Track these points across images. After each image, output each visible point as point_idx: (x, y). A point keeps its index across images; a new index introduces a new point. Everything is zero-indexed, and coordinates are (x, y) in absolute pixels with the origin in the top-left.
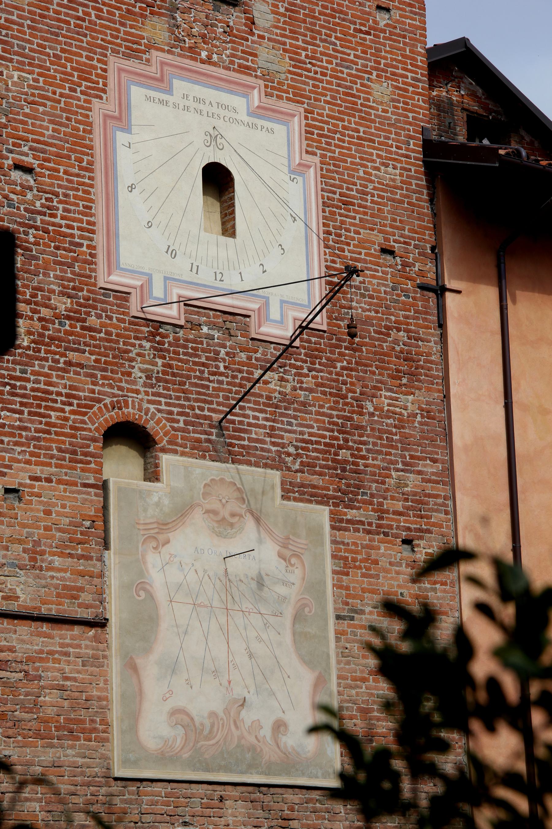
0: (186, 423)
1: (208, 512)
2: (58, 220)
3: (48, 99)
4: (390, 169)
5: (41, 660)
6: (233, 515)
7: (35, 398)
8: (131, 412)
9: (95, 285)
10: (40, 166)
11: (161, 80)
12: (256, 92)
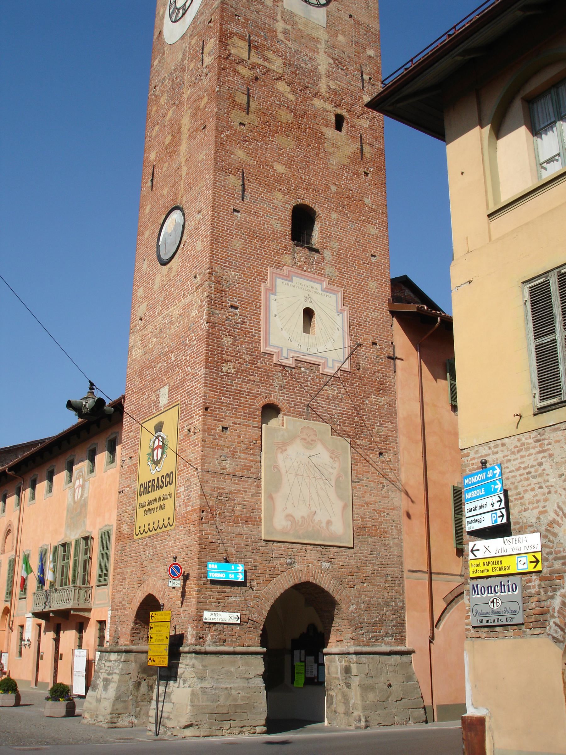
0: (295, 405)
1: (302, 439)
2: (247, 326)
3: (245, 282)
4: (376, 313)
5: (235, 493)
6: (312, 441)
7: (235, 393)
8: (272, 400)
9: (260, 351)
10: (241, 306)
11: (288, 277)
12: (325, 283)
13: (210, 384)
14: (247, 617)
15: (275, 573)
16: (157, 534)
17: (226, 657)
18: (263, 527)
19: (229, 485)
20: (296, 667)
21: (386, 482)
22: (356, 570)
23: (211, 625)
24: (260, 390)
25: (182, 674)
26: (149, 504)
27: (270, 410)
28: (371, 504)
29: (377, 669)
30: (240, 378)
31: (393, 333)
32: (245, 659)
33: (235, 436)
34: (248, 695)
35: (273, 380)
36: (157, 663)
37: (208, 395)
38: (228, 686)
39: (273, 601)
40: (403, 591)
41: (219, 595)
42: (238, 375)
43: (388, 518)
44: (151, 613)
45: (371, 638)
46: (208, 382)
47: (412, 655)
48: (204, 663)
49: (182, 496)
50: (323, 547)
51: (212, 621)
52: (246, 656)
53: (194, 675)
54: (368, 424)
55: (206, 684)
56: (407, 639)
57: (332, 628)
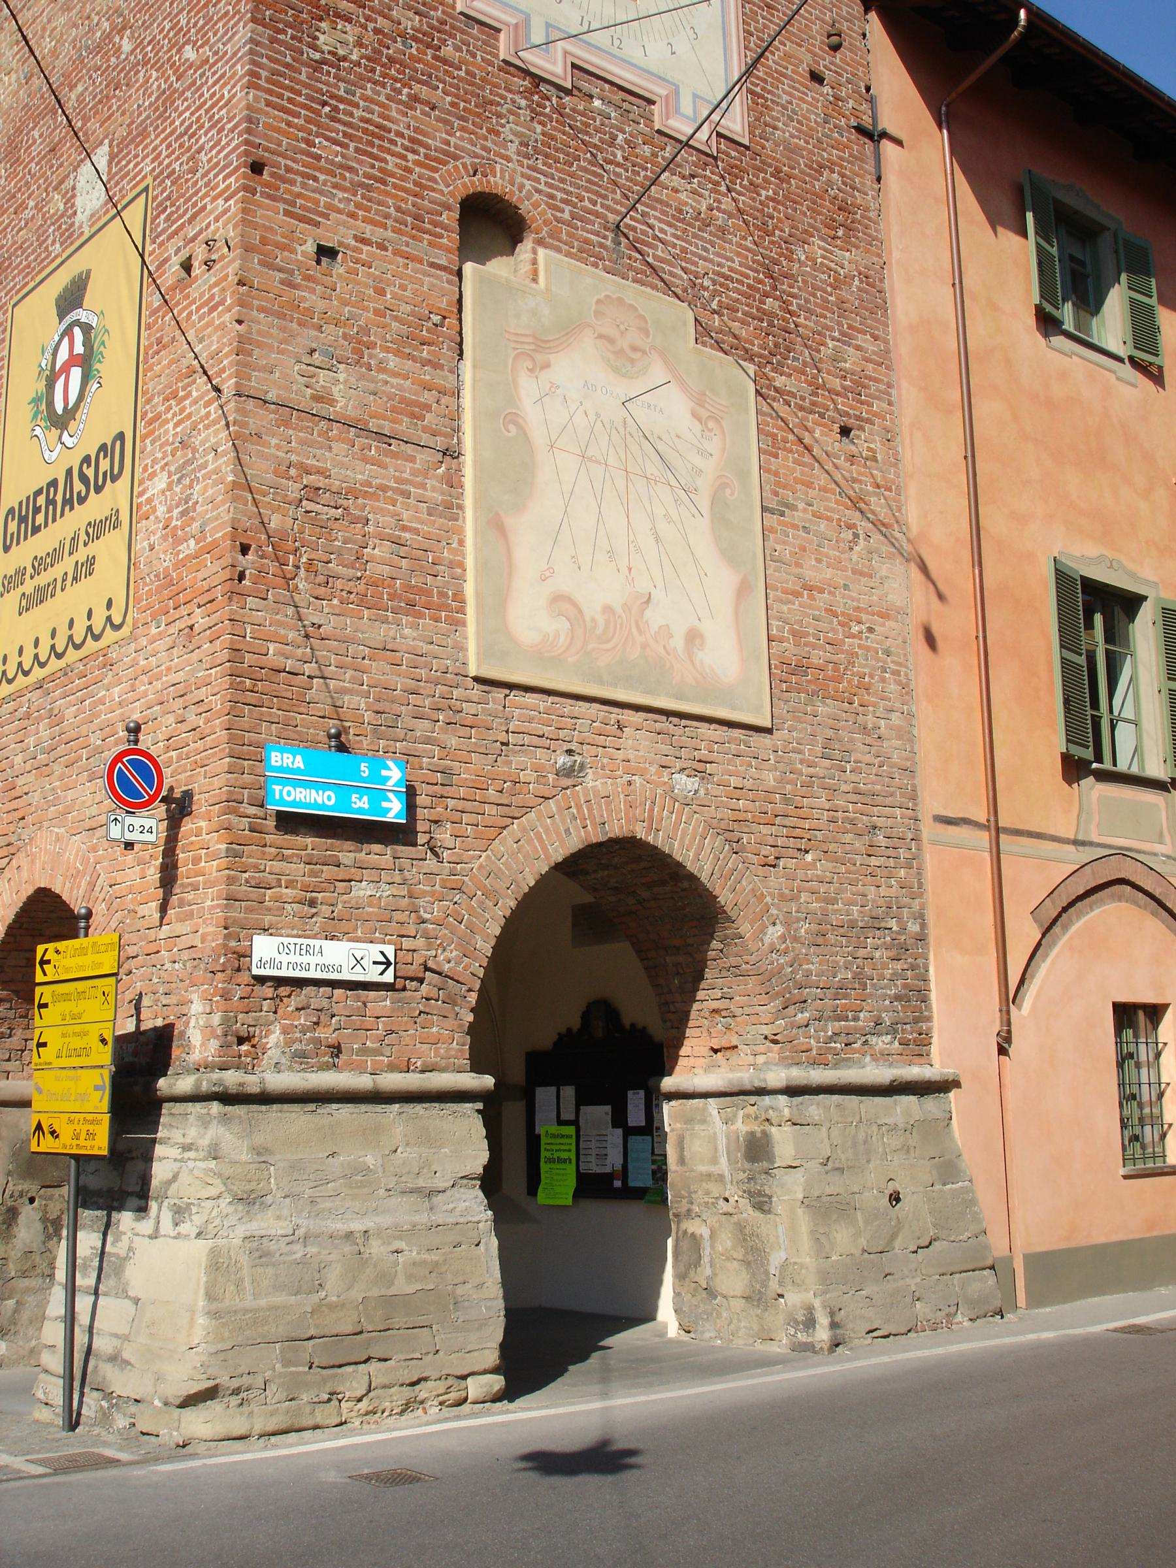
0: (573, 216)
1: (600, 337)
6: (635, 349)
7: (365, 131)
9: (454, 8)
13: (268, 80)
14: (418, 959)
15: (517, 800)
16: (65, 671)
17: (344, 1112)
18: (471, 629)
19: (342, 462)
20: (543, 1140)
21: (863, 525)
22: (780, 808)
23: (284, 991)
24: (453, 140)
25: (169, 1183)
26: (37, 572)
27: (490, 223)
28: (822, 591)
29: (854, 1145)
30: (384, 86)
31: (870, 58)
32: (417, 1116)
33: (366, 286)
34: (434, 1257)
35: (499, 116)
36: (66, 1144)
37: (263, 119)
38: (357, 1226)
39: (513, 904)
40: (920, 885)
41: (313, 874)
42: (373, 71)
43: (872, 641)
44: (40, 949)
45: (831, 1039)
46: (264, 74)
47: (951, 1095)
48: (259, 1139)
49: (161, 510)
50: (675, 720)
51: (284, 973)
52: (419, 1109)
53: (218, 1188)
54: (806, 327)
55: (271, 1223)
56: (935, 1040)
57: (696, 1006)
